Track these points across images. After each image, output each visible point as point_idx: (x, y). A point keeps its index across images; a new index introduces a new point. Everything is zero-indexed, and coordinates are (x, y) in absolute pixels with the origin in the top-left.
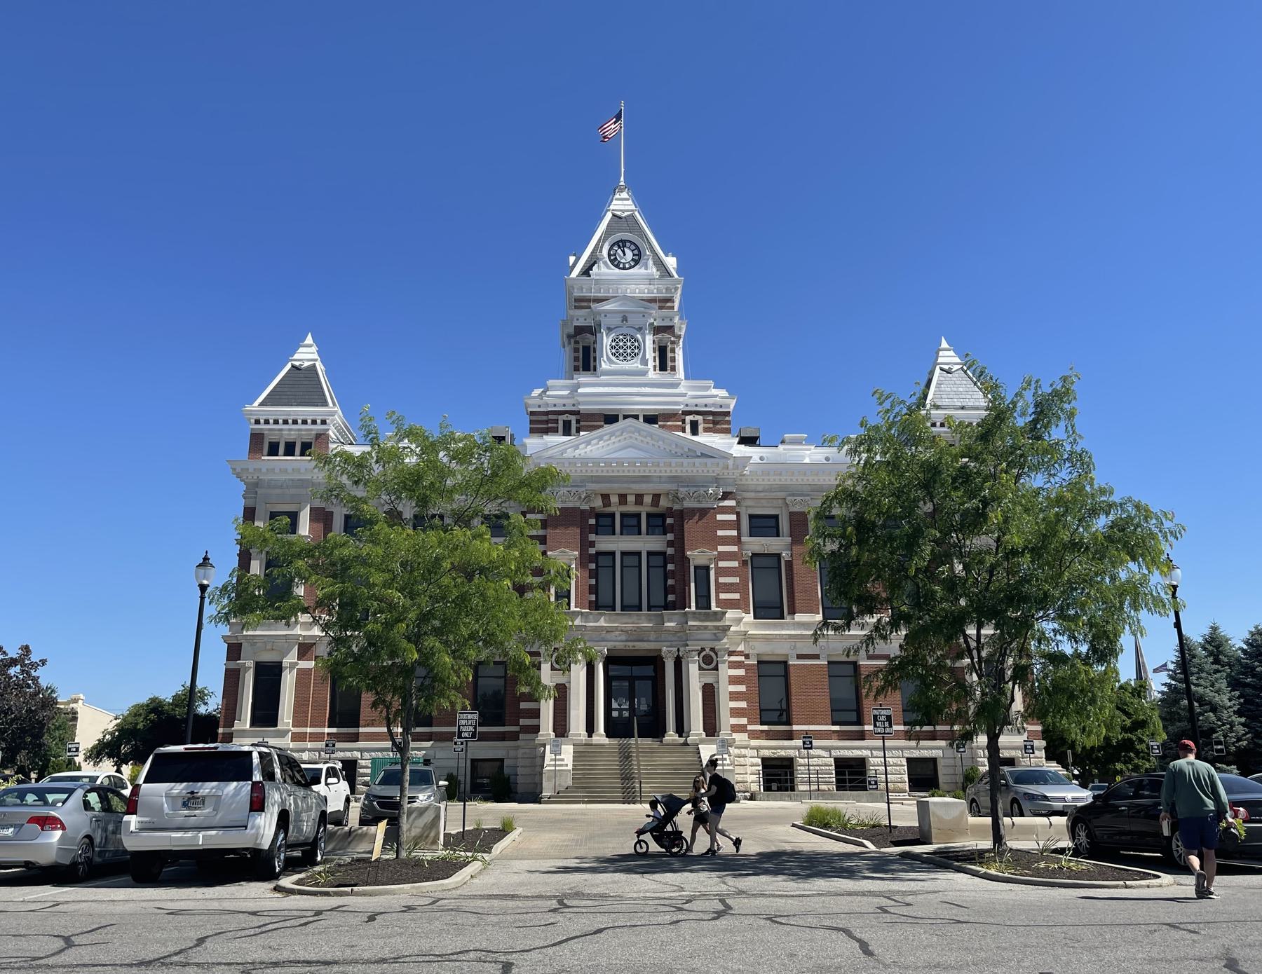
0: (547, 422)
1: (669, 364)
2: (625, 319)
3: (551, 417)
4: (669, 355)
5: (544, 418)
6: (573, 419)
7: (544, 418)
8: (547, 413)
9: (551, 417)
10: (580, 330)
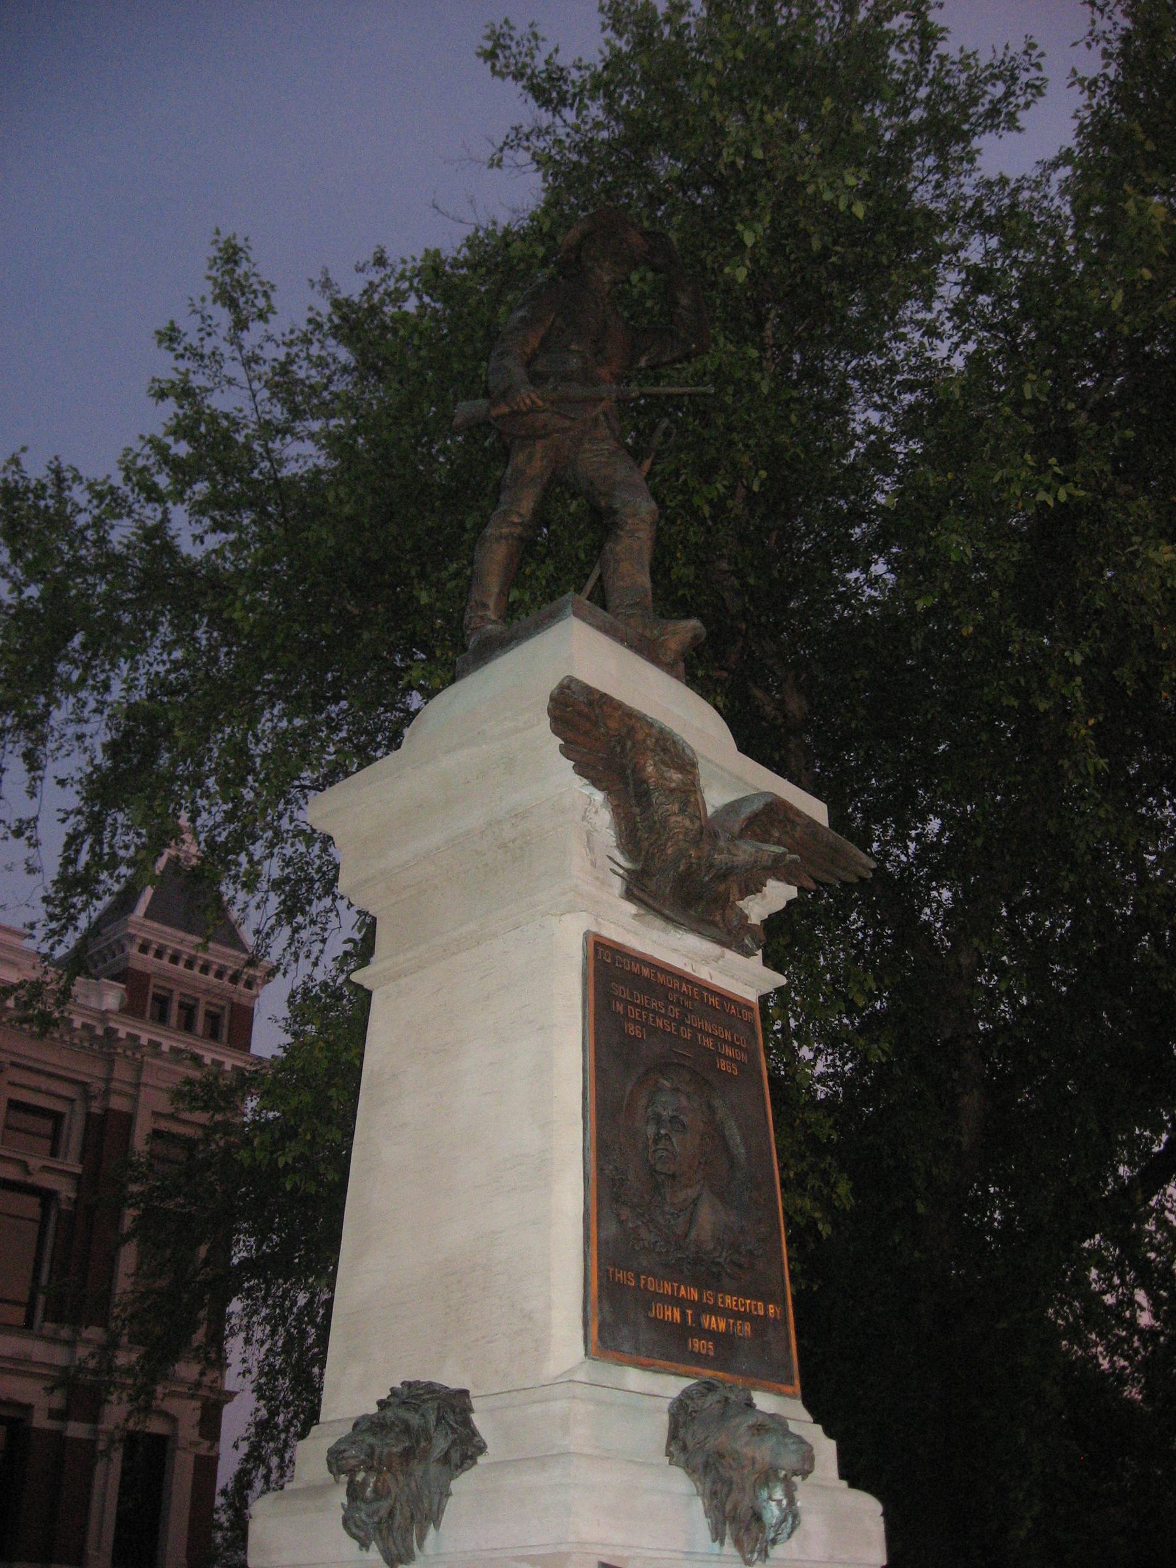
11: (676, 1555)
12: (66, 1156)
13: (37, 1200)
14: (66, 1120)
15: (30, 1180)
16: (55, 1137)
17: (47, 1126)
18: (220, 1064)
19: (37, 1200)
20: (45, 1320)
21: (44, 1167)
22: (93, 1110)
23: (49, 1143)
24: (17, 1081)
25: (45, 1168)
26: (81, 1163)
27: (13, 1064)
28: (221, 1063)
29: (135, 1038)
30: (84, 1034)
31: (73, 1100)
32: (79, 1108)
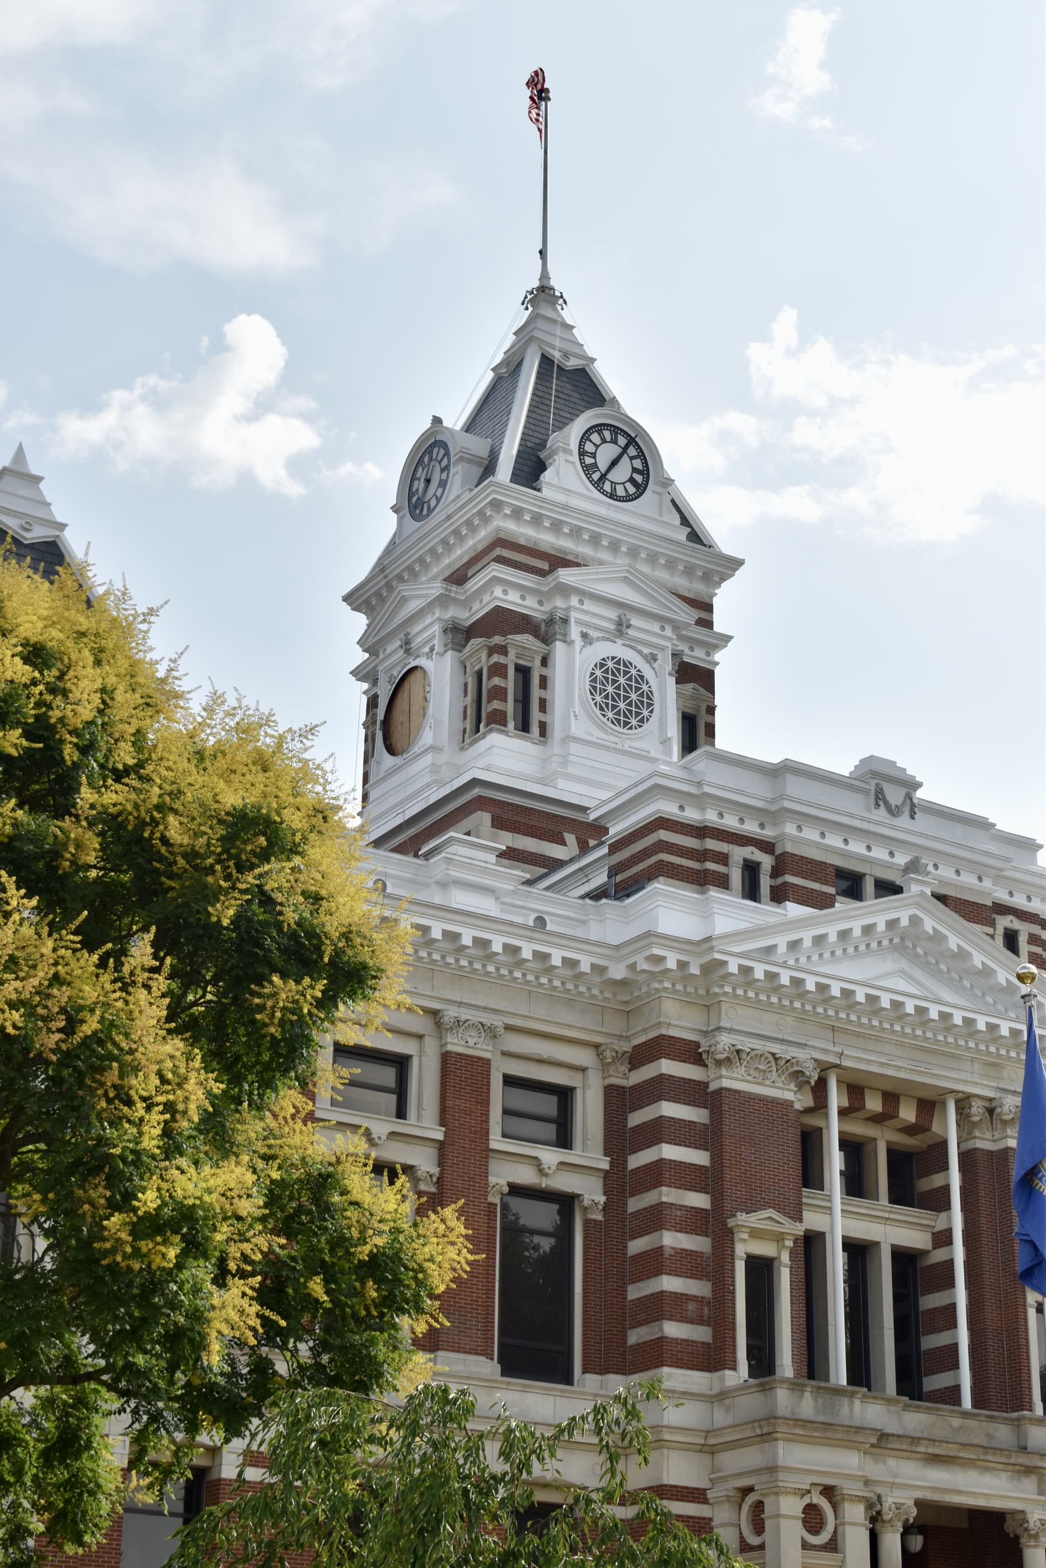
0: (703, 855)
1: (536, 716)
3: (711, 844)
4: (536, 693)
6: (766, 862)
8: (702, 831)
9: (711, 844)
10: (501, 622)
11: (696, 1447)
12: (419, 1118)
13: (556, 1207)
14: (415, 1063)
15: (545, 1183)
16: (401, 1090)
17: (387, 1075)
18: (545, 957)
19: (556, 1207)
20: (585, 1371)
21: (562, 1163)
22: (450, 1048)
23: (393, 1098)
24: (514, 1049)
25: (393, 1134)
26: (442, 1124)
27: (509, 1028)
28: (517, 950)
29: (514, 950)
30: (567, 972)
31: (420, 1037)
32: (431, 1047)
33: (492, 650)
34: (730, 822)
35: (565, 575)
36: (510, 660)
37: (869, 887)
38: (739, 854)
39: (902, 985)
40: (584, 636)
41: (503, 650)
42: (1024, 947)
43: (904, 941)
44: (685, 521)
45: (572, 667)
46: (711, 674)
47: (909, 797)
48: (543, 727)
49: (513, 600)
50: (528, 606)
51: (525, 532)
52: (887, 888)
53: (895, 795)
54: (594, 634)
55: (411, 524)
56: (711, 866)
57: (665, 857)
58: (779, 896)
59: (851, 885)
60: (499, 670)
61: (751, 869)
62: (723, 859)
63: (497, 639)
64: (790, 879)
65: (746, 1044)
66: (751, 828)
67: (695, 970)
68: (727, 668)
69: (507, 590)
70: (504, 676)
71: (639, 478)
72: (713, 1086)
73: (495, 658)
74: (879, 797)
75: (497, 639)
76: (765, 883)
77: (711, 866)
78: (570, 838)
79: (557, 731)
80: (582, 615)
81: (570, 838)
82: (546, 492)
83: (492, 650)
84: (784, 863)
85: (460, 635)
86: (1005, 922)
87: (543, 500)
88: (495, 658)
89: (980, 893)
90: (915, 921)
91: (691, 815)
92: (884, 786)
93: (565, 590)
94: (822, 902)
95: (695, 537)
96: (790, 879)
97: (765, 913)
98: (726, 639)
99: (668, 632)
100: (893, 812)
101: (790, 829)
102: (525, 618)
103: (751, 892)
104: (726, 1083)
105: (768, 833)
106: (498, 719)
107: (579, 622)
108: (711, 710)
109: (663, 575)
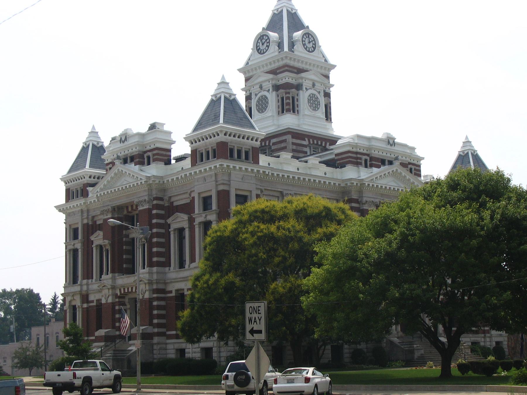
0: (357, 158)
1: (296, 109)
2: (314, 85)
3: (359, 156)
4: (296, 103)
5: (354, 155)
6: (368, 158)
7: (354, 155)
8: (357, 153)
9: (359, 156)
10: (287, 86)
33: (286, 93)
34: (361, 151)
35: (303, 75)
36: (290, 96)
37: (387, 163)
38: (364, 157)
39: (395, 185)
40: (306, 88)
41: (289, 93)
42: (413, 171)
43: (394, 174)
44: (324, 57)
45: (303, 97)
46: (330, 94)
47: (394, 141)
48: (298, 111)
49: (290, 81)
50: (293, 82)
51: (292, 63)
52: (391, 163)
53: (391, 142)
54: (308, 88)
55: (257, 55)
56: (359, 161)
57: (350, 159)
58: (371, 166)
59: (383, 162)
60: (288, 98)
61: (366, 161)
62: (361, 159)
63: (288, 91)
64: (373, 162)
65: (368, 199)
66: (365, 152)
67: (359, 185)
68: (333, 92)
69: (287, 78)
70: (290, 100)
71: (314, 46)
72: (361, 208)
73: (287, 95)
74: (389, 142)
75: (288, 91)
76: (368, 163)
77: (359, 161)
78: (306, 139)
79: (301, 112)
80: (306, 84)
81: (306, 139)
82: (296, 53)
83: (286, 93)
84: (372, 159)
85: (277, 88)
86: (410, 166)
87: (295, 55)
88: (287, 95)
89: (406, 161)
90: (397, 170)
91: (354, 150)
92: (390, 141)
93: (302, 78)
94: (379, 167)
95: (326, 60)
96: (373, 162)
97: (369, 170)
98: (333, 86)
99: (322, 86)
100: (391, 145)
101: (373, 152)
102: (292, 84)
103: (366, 166)
104: (364, 208)
105: (368, 152)
106: (288, 110)
107: (305, 85)
108: (330, 103)
109: (319, 70)
